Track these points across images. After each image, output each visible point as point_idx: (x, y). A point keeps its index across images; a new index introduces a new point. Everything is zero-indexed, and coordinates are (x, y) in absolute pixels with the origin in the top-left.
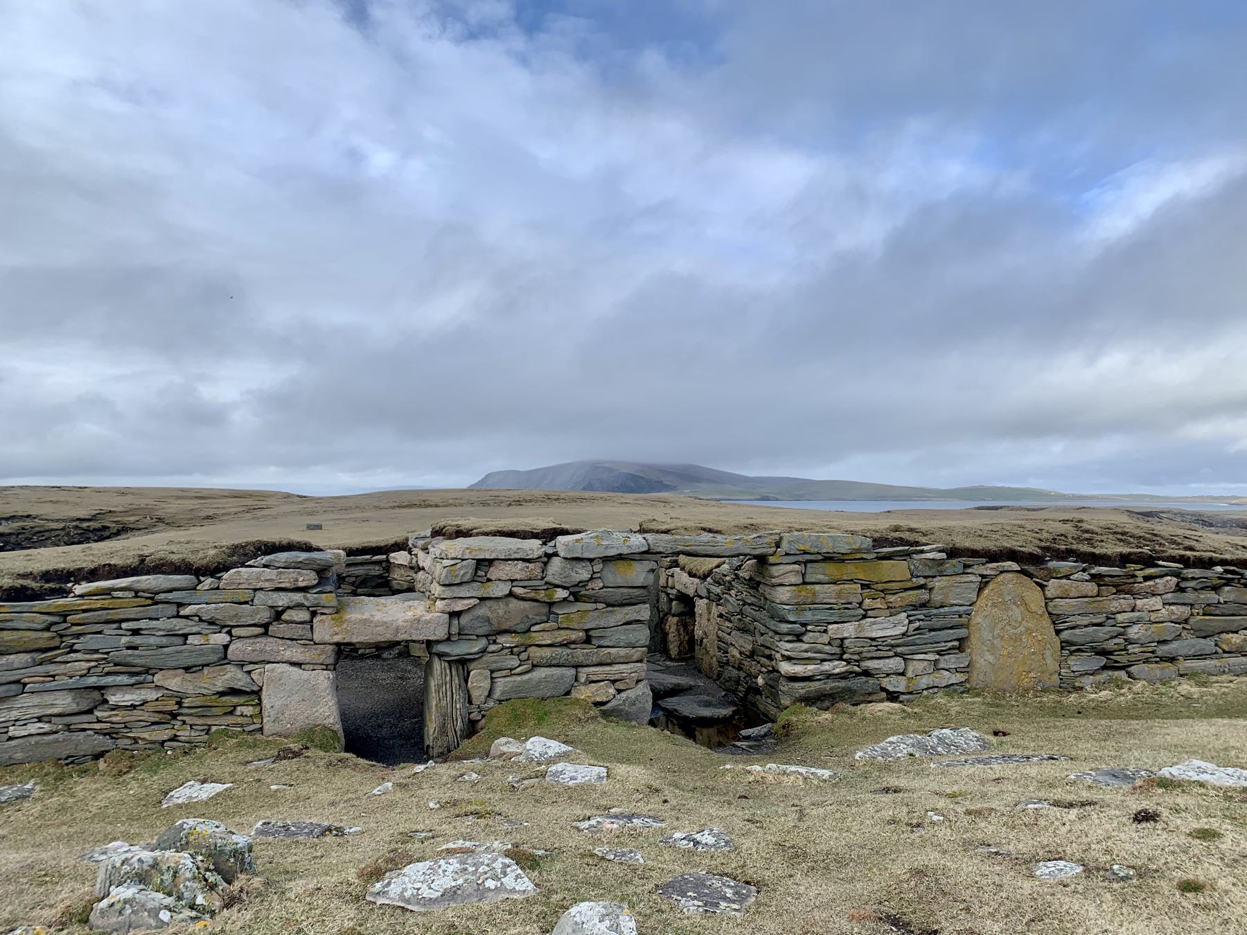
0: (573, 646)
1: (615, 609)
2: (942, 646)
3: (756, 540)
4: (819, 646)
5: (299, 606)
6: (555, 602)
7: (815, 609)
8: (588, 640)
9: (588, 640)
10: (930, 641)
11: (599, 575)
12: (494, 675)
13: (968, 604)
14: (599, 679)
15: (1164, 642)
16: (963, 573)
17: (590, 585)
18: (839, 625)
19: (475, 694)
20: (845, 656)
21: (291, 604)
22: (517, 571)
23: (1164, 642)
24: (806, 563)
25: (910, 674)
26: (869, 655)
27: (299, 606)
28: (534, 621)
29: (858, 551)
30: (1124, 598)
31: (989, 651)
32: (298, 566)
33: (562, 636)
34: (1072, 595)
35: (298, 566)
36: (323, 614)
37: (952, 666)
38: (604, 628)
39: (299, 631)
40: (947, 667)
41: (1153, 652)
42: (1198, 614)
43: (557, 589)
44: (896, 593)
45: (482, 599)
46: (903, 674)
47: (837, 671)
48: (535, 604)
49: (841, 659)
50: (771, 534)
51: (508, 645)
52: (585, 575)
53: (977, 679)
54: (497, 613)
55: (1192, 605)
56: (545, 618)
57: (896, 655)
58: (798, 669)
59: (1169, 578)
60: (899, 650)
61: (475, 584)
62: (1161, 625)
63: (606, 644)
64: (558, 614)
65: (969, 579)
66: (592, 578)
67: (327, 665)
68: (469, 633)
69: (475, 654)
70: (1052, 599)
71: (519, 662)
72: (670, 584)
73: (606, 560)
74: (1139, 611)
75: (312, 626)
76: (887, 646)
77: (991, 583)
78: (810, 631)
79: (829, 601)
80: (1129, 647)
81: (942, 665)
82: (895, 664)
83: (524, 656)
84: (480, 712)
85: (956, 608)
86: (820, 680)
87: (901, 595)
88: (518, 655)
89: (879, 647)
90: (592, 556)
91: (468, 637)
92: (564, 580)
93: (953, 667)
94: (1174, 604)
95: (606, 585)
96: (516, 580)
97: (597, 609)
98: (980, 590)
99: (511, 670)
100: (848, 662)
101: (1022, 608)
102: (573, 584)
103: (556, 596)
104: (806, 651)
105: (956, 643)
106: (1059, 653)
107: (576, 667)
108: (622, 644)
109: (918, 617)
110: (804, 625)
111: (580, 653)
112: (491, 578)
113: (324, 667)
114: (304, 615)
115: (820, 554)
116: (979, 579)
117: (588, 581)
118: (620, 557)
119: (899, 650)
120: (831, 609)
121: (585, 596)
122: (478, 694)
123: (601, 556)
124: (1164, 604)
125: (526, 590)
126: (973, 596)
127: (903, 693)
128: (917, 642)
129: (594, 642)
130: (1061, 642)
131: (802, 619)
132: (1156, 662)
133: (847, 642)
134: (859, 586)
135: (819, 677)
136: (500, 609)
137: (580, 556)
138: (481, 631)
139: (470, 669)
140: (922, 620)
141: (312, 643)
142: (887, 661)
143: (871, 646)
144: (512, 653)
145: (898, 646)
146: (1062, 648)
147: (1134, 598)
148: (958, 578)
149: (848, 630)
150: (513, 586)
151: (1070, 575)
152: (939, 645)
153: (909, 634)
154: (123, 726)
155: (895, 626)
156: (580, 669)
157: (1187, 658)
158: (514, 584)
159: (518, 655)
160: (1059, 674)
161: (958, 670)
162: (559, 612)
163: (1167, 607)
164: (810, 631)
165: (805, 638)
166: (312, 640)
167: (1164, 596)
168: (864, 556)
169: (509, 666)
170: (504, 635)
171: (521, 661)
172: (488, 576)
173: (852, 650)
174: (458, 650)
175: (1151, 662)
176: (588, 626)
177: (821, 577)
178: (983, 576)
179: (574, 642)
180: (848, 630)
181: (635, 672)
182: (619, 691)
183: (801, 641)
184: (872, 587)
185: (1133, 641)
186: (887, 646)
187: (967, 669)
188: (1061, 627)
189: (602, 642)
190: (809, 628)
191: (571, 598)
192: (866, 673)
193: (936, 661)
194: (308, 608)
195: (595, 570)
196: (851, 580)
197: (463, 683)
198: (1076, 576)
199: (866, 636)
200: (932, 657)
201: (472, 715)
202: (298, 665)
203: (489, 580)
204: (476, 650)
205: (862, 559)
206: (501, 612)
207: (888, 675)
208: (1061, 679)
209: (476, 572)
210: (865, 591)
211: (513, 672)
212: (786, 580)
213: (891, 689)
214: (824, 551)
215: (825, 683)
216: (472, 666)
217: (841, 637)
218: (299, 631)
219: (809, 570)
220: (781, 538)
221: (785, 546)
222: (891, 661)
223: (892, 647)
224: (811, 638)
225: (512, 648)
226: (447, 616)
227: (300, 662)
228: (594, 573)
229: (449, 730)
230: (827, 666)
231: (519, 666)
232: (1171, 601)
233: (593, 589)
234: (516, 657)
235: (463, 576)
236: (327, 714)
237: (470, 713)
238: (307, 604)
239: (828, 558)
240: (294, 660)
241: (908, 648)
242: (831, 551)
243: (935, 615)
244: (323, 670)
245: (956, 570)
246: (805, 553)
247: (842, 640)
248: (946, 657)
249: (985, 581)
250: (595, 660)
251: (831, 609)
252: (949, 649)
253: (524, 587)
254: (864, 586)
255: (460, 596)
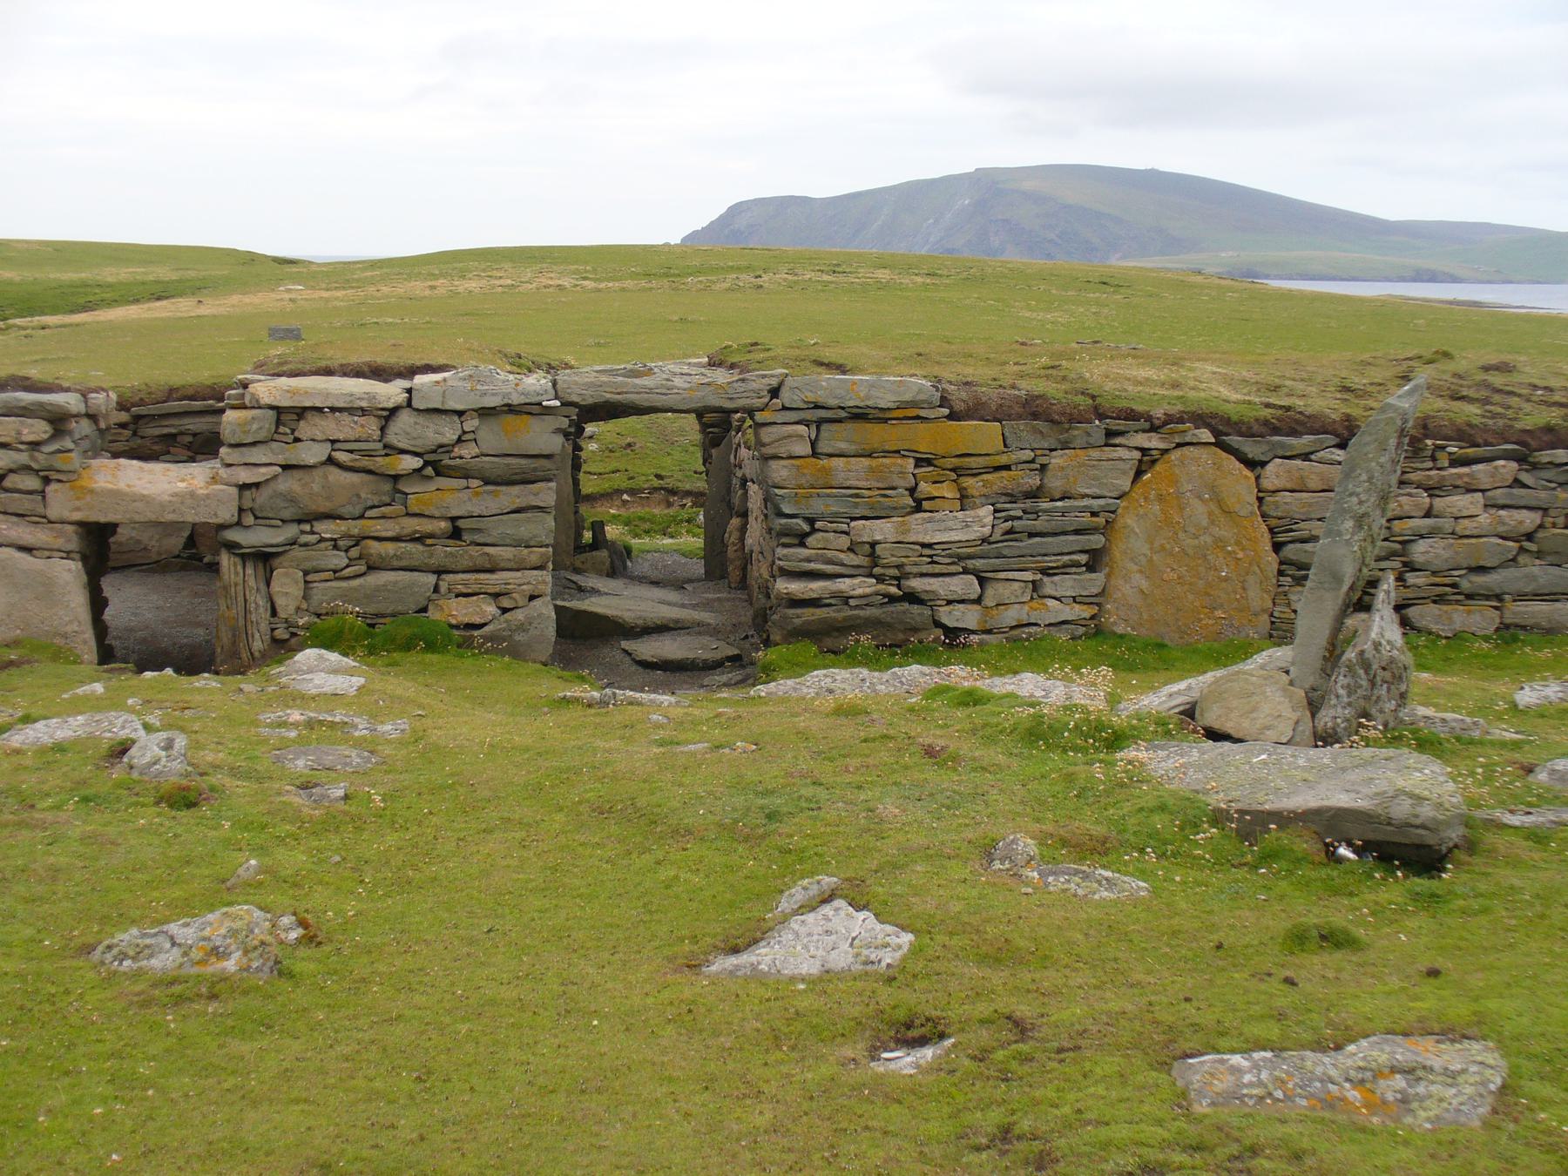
0: (429, 541)
1: (498, 488)
2: (1051, 562)
3: (735, 385)
4: (829, 554)
5: (26, 469)
6: (402, 476)
7: (828, 496)
8: (456, 534)
9: (456, 534)
10: (1029, 552)
11: (470, 436)
12: (309, 578)
13: (1115, 494)
14: (470, 591)
15: (1481, 569)
16: (1107, 445)
17: (457, 451)
18: (867, 523)
19: (280, 602)
20: (877, 570)
21: (13, 466)
22: (345, 428)
23: (1481, 569)
24: (820, 423)
25: (989, 601)
26: (915, 570)
27: (26, 469)
28: (370, 503)
29: (914, 404)
30: (1409, 495)
31: (1141, 572)
32: (24, 412)
33: (412, 525)
34: (1312, 485)
35: (24, 412)
36: (60, 481)
37: (1064, 594)
38: (480, 516)
39: (25, 503)
40: (1058, 594)
41: (1454, 586)
42: (1554, 525)
43: (400, 456)
44: (981, 474)
45: (285, 467)
46: (978, 601)
47: (859, 591)
48: (370, 477)
49: (871, 575)
50: (764, 376)
51: (328, 536)
52: (450, 435)
53: (1115, 620)
54: (310, 490)
55: (1545, 510)
56: (386, 499)
57: (966, 571)
58: (795, 587)
59: (1502, 462)
60: (970, 564)
61: (274, 445)
62: (1473, 541)
63: (482, 540)
64: (407, 494)
65: (1115, 455)
66: (459, 440)
67: (68, 552)
68: (270, 515)
69: (277, 546)
70: (591, 498)
71: (347, 561)
72: (814, 427)
73: (485, 413)
74: (1437, 517)
75: (44, 497)
76: (950, 556)
77: (1159, 462)
78: (819, 530)
79: (860, 484)
80: (1408, 575)
81: (1048, 590)
82: (964, 585)
83: (354, 552)
84: (287, 628)
85: (1086, 502)
86: (829, 605)
87: (985, 477)
88: (346, 551)
89: (935, 559)
90: (460, 407)
91: (268, 522)
92: (413, 442)
93: (1068, 594)
94: (1503, 507)
95: (485, 451)
96: (338, 441)
97: (468, 488)
98: (1139, 473)
99: (335, 572)
100: (880, 579)
101: (1213, 506)
102: (428, 449)
103: (400, 467)
104: (809, 560)
105: (1083, 558)
106: (1274, 581)
107: (439, 572)
108: (508, 541)
109: (1012, 513)
110: (811, 521)
111: (443, 552)
112: (300, 437)
113: (64, 555)
114: (32, 483)
115: (843, 408)
116: (1137, 455)
117: (453, 446)
118: (510, 409)
119: (970, 564)
120: (857, 496)
121: (449, 467)
122: (286, 606)
123: (474, 407)
124: (1486, 506)
125: (353, 456)
126: (1125, 483)
127: (974, 632)
128: (1005, 552)
129: (467, 537)
130: (1281, 563)
131: (807, 512)
132: (1457, 602)
133: (878, 547)
134: (911, 461)
135: (827, 601)
136: (316, 482)
137: (440, 407)
138: (286, 514)
139: (274, 566)
140: (1020, 518)
141: (44, 520)
142: (947, 579)
143: (921, 556)
144: (336, 547)
145: (970, 557)
146: (1281, 573)
147: (1430, 496)
148: (1095, 454)
149: (881, 530)
150: (333, 450)
151: (1312, 453)
152: (1046, 558)
153: (992, 539)
154: (1000, 264)
155: (967, 526)
156: (444, 576)
157: (1521, 597)
158: (338, 446)
159: (346, 551)
160: (1272, 615)
161: (1078, 599)
162: (407, 491)
163: (1493, 511)
164: (819, 530)
165: (810, 541)
166: (45, 517)
167: (1489, 494)
168: (923, 413)
169: (333, 567)
170: (326, 521)
171: (350, 560)
172: (296, 434)
173: (885, 561)
174: (255, 537)
175: (1449, 602)
176: (455, 513)
177: (842, 446)
178: (1144, 451)
179: (431, 536)
180: (881, 530)
181: (529, 583)
182: (505, 610)
183: (802, 545)
184: (935, 462)
185: (1417, 567)
186: (950, 556)
187: (1097, 600)
188: (1281, 538)
189: (479, 538)
190: (818, 525)
191: (429, 471)
192: (912, 598)
193: (1035, 585)
194: (38, 471)
195: (466, 429)
196: (898, 452)
197: (263, 586)
198: (1320, 454)
199: (911, 540)
200: (1028, 576)
201: (277, 633)
202: (27, 549)
203: (297, 440)
204: (280, 540)
205: (918, 417)
206: (316, 487)
207: (949, 602)
208: (1273, 623)
209: (277, 427)
210: (923, 470)
211: (337, 575)
212: (783, 450)
213: (951, 623)
214: (851, 403)
215: (839, 611)
216: (276, 562)
217: (869, 540)
218: (25, 503)
219: (823, 434)
220: (781, 384)
221: (786, 397)
222: (955, 580)
223: (961, 559)
224: (818, 541)
225: (335, 540)
226: (234, 491)
227: (31, 546)
228: (464, 432)
229: (243, 651)
230: (844, 585)
231: (347, 566)
232: (1501, 502)
233: (461, 458)
234: (343, 554)
235: (256, 432)
236: (67, 619)
237: (273, 630)
238: (35, 466)
239: (859, 415)
240: (21, 543)
241: (986, 561)
242: (861, 404)
243: (1045, 511)
244: (62, 558)
245: (1092, 441)
246: (817, 407)
247: (873, 545)
248: (1056, 578)
249: (1146, 461)
250: (466, 563)
251: (857, 496)
252: (1064, 566)
253: (351, 452)
254: (919, 462)
255: (252, 462)
